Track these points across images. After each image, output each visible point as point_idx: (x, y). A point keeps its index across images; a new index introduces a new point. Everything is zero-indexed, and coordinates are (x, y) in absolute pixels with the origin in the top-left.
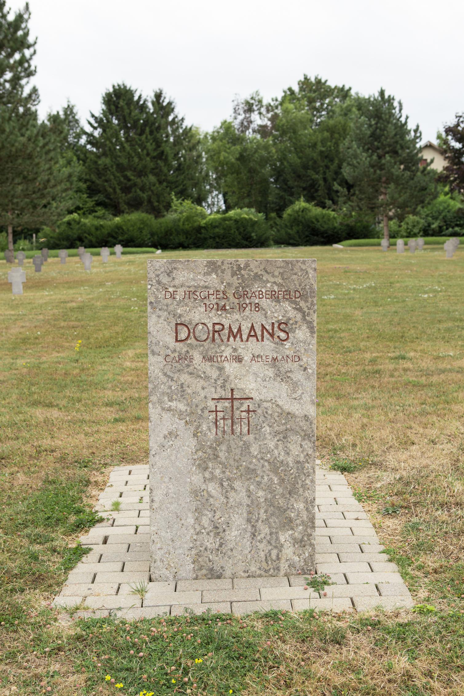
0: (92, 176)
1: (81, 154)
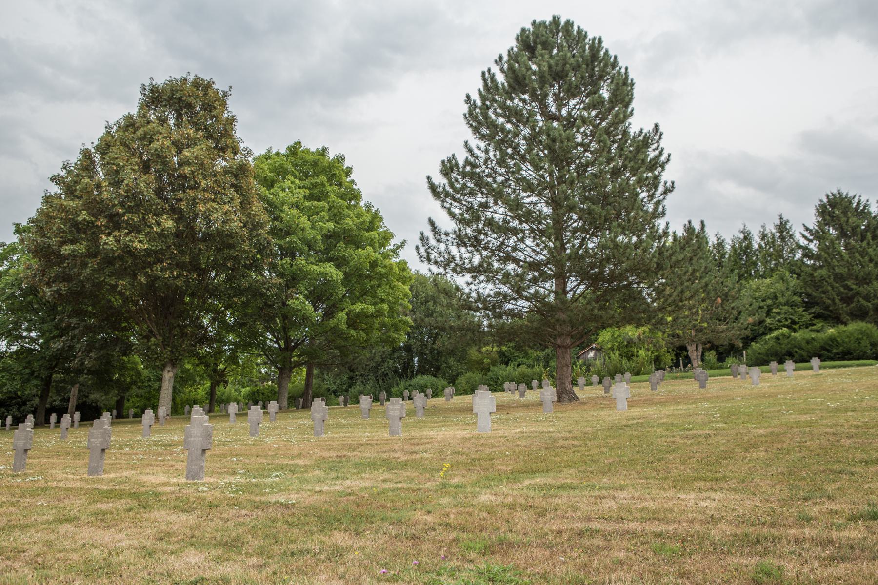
0: (808, 289)
1: (796, 269)
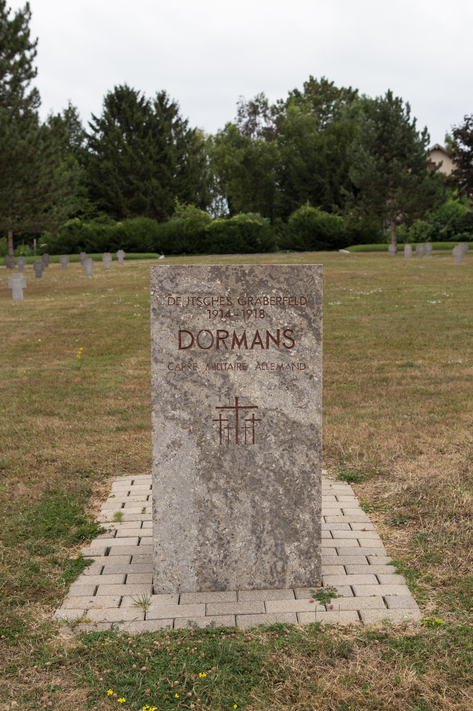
0: (94, 180)
1: (83, 157)
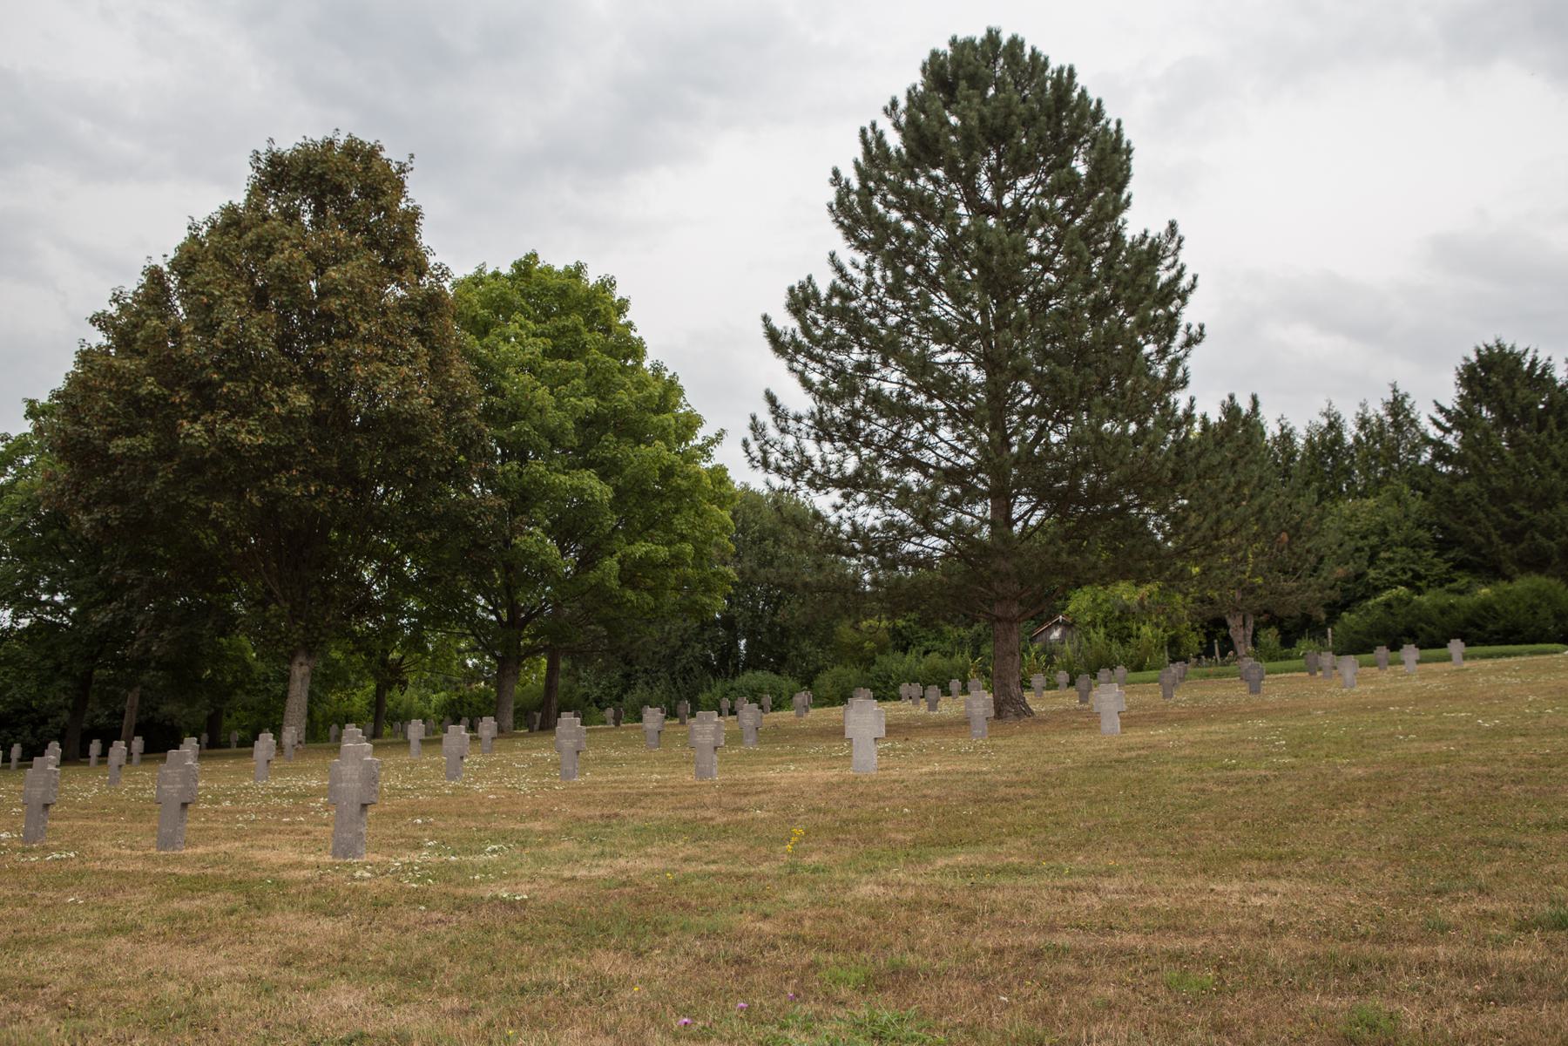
0: (1443, 517)
1: (1421, 480)
